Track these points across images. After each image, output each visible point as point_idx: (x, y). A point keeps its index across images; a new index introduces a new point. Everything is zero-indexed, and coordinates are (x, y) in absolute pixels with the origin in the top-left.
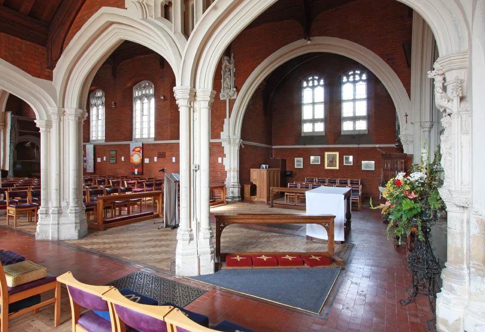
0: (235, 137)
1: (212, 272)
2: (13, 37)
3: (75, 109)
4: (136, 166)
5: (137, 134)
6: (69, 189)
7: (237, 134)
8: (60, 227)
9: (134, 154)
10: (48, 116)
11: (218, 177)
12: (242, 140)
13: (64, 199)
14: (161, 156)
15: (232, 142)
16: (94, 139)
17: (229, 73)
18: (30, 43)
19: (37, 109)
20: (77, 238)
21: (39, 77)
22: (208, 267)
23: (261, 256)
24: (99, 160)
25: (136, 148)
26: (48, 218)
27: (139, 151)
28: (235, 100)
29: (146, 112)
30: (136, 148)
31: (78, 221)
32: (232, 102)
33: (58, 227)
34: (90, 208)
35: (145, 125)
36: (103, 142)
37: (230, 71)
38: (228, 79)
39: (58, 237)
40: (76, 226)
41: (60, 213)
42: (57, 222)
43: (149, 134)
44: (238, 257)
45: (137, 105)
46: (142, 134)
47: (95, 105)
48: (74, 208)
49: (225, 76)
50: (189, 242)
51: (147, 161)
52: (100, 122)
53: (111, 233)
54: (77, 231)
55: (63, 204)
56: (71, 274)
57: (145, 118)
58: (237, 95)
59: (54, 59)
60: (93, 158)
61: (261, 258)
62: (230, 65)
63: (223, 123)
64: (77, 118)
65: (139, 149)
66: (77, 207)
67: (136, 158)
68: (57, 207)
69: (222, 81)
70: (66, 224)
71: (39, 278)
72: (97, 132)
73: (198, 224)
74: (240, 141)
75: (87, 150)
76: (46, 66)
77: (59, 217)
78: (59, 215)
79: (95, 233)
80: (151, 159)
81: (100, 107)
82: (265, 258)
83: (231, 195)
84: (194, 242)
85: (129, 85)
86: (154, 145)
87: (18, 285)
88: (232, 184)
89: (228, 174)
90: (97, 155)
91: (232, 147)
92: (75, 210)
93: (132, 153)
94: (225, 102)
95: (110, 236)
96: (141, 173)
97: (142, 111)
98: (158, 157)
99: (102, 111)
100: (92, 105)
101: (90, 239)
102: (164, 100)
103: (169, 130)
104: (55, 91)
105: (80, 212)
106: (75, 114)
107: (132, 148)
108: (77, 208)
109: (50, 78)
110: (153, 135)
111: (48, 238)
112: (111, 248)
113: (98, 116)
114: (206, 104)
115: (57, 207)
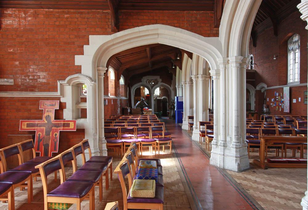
2: (192, 11)
3: (236, 57)
6: (232, 126)
8: (225, 157)
10: (217, 66)
13: (228, 135)
16: (291, 81)
18: (202, 12)
19: (210, 62)
20: (237, 170)
21: (209, 36)
24: (294, 101)
26: (217, 148)
31: (239, 155)
33: (224, 158)
34: (253, 145)
36: (298, 84)
39: (224, 166)
40: (236, 160)
41: (225, 146)
42: (223, 153)
47: (292, 50)
48: (235, 144)
53: (269, 174)
54: (237, 164)
55: (228, 139)
59: (218, 19)
60: (289, 99)
64: (238, 65)
66: (238, 143)
68: (223, 141)
70: (229, 156)
71: (148, 197)
72: (294, 75)
75: (284, 92)
76: (214, 26)
77: (224, 150)
78: (225, 147)
79: (255, 170)
87: (135, 197)
90: (293, 96)
92: (236, 145)
95: (266, 176)
99: (298, 54)
100: (289, 50)
101: (246, 174)
104: (221, 44)
105: (240, 148)
106: (236, 61)
108: (237, 144)
109: (217, 35)
111: (217, 165)
112: (257, 189)
113: (295, 60)
115: (223, 141)
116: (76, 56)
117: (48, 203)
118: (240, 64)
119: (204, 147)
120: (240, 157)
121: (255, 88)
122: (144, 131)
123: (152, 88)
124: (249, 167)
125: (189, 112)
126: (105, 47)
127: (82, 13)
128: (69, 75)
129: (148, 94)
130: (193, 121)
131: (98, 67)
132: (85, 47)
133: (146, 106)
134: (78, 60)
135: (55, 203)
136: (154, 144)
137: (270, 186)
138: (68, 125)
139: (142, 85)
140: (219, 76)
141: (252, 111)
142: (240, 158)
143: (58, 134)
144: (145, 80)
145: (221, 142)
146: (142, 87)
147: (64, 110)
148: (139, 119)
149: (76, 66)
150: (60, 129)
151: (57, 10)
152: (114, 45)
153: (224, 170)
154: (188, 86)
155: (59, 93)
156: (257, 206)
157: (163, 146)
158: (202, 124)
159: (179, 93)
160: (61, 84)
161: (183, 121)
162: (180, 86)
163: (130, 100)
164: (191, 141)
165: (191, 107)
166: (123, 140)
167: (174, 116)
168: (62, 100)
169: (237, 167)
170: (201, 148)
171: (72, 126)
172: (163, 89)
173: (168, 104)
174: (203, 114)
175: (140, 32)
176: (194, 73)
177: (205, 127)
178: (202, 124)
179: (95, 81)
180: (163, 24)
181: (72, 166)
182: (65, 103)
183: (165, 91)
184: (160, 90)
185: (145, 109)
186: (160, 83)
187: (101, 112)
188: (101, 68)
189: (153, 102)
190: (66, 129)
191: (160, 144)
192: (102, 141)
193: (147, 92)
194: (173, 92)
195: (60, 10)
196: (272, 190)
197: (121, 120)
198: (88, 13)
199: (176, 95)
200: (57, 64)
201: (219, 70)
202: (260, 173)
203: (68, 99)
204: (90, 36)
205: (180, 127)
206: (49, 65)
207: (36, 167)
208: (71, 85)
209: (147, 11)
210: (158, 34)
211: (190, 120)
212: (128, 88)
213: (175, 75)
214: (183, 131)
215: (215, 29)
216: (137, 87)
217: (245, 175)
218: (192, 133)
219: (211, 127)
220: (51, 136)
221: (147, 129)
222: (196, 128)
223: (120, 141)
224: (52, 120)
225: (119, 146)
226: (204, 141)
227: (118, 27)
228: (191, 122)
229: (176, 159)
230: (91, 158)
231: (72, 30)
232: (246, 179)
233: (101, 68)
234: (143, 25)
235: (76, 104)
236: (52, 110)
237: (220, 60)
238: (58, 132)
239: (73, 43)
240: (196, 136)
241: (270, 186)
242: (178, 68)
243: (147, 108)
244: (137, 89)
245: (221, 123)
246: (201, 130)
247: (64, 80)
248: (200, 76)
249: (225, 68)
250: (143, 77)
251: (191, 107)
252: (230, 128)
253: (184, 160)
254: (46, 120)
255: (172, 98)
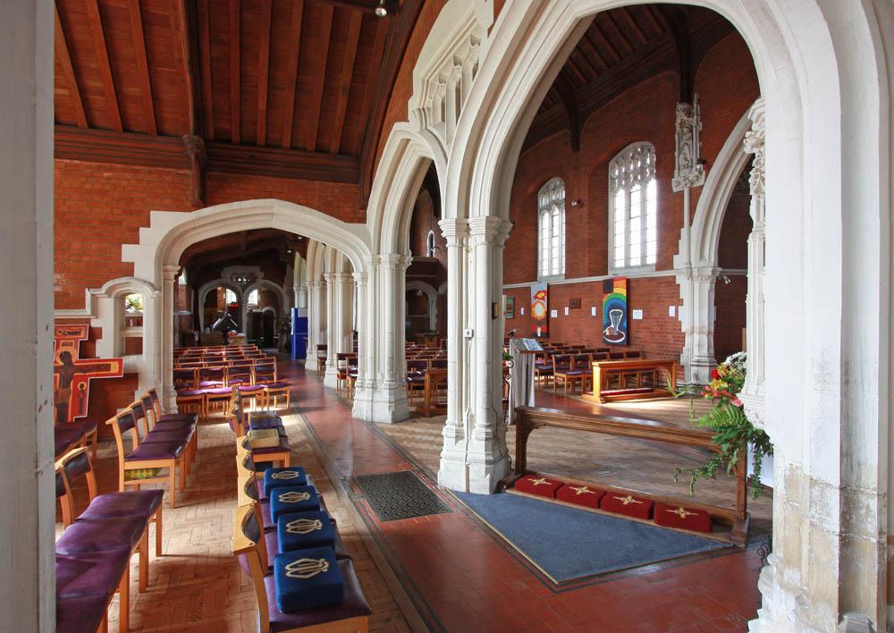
0: (702, 264)
1: (487, 492)
4: (539, 323)
5: (618, 259)
7: (707, 257)
9: (536, 303)
11: (669, 344)
12: (720, 269)
14: (576, 305)
15: (695, 273)
17: (689, 135)
20: (390, 422)
22: (481, 484)
23: (677, 508)
25: (539, 292)
27: (543, 299)
28: (701, 187)
29: (636, 211)
30: (539, 292)
32: (695, 193)
35: (636, 238)
36: (563, 281)
37: (691, 131)
38: (686, 147)
41: (374, 387)
42: (375, 405)
43: (644, 257)
44: (682, 510)
45: (618, 201)
46: (551, 269)
49: (682, 143)
50: (456, 442)
51: (554, 314)
52: (556, 241)
55: (379, 377)
56: (276, 445)
57: (636, 224)
58: (706, 179)
61: (676, 512)
62: (690, 119)
63: (679, 237)
64: (394, 267)
65: (543, 294)
67: (539, 311)
69: (676, 153)
73: (471, 418)
74: (714, 272)
80: (561, 312)
81: (557, 211)
82: (683, 514)
83: (693, 381)
84: (462, 443)
85: (531, 189)
86: (651, 280)
88: (697, 358)
89: (687, 340)
91: (697, 285)
93: (533, 301)
94: (681, 194)
95: (429, 425)
96: (546, 334)
97: (629, 209)
98: (570, 308)
102: (579, 207)
103: (587, 259)
104: (370, 236)
107: (533, 293)
109: (363, 220)
110: (652, 259)
112: (409, 440)
113: (552, 230)
114: (483, 238)
116: (124, 246)
117: (125, 471)
118: (397, 266)
119: (344, 395)
120: (395, 402)
121: (437, 290)
122: (241, 373)
123: (243, 291)
124: (408, 416)
125: (318, 338)
126: (181, 230)
127: (137, 172)
128: (108, 279)
129: (232, 303)
130: (326, 353)
131: (164, 265)
132: (143, 231)
133: (234, 328)
134: (128, 253)
135: (136, 470)
136: (260, 395)
137: (431, 435)
138: (107, 367)
139: (221, 285)
140: (367, 281)
141: (432, 331)
142: (396, 402)
143: (87, 386)
144: (227, 273)
145: (368, 382)
146: (220, 288)
147: (98, 341)
148: (224, 353)
149: (124, 263)
150: (90, 376)
151: (88, 163)
152: (195, 228)
153: (372, 423)
154: (317, 289)
155: (88, 311)
156: (408, 456)
157: (275, 397)
158: (341, 357)
159: (299, 302)
160: (93, 295)
161: (308, 355)
162: (302, 288)
163: (195, 316)
164: (322, 388)
165: (323, 328)
166: (205, 391)
167: (288, 347)
168: (95, 324)
169: (390, 417)
170: (340, 398)
171: (115, 368)
172: (263, 292)
173: (275, 321)
174: (343, 340)
175: (241, 209)
176: (329, 269)
177: (346, 362)
178: (341, 357)
179: (160, 290)
180: (281, 199)
181: (115, 440)
182: (100, 329)
183: (269, 297)
184: (259, 293)
185: (232, 334)
186: (260, 281)
187: (168, 343)
188: (170, 267)
189: (245, 319)
190: (103, 375)
191: (272, 394)
192: (169, 393)
193: (231, 297)
194: (286, 300)
195: (94, 164)
196: (432, 438)
197: (188, 356)
198: (150, 173)
199: (292, 304)
200: (86, 259)
201: (367, 273)
202: (422, 422)
203: (106, 321)
204: (152, 212)
205: (302, 366)
206: (69, 260)
207: (107, 423)
208: (113, 296)
209: (255, 177)
210: (272, 214)
211: (320, 351)
212: (193, 292)
213: (293, 267)
214: (306, 373)
215: (361, 211)
216: (210, 290)
217: (401, 427)
218: (324, 375)
219: (354, 362)
220: (72, 387)
221: (247, 370)
222: (332, 365)
223: (199, 392)
224: (74, 360)
225: (196, 401)
226: (344, 387)
227: (205, 200)
228: (322, 356)
229: (298, 416)
230: (161, 417)
231: (117, 200)
232: (401, 431)
233: (170, 267)
234: (247, 198)
235: (121, 329)
236: (73, 341)
237: (368, 258)
238: (87, 382)
239: (120, 223)
240: (331, 379)
241: (431, 435)
242: (298, 255)
243: (234, 331)
244: (212, 291)
245: (369, 353)
246: (340, 367)
247: (100, 286)
248: (338, 275)
249: (375, 270)
250: (225, 269)
251: (323, 328)
252: (382, 359)
253: (313, 417)
254: (62, 361)
255: (286, 309)
